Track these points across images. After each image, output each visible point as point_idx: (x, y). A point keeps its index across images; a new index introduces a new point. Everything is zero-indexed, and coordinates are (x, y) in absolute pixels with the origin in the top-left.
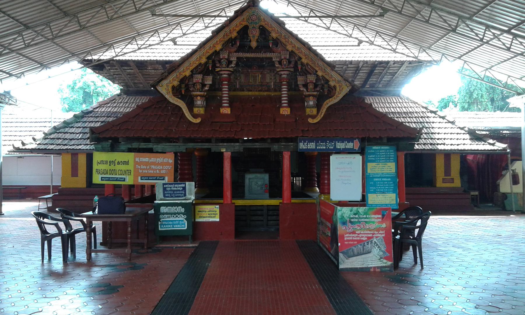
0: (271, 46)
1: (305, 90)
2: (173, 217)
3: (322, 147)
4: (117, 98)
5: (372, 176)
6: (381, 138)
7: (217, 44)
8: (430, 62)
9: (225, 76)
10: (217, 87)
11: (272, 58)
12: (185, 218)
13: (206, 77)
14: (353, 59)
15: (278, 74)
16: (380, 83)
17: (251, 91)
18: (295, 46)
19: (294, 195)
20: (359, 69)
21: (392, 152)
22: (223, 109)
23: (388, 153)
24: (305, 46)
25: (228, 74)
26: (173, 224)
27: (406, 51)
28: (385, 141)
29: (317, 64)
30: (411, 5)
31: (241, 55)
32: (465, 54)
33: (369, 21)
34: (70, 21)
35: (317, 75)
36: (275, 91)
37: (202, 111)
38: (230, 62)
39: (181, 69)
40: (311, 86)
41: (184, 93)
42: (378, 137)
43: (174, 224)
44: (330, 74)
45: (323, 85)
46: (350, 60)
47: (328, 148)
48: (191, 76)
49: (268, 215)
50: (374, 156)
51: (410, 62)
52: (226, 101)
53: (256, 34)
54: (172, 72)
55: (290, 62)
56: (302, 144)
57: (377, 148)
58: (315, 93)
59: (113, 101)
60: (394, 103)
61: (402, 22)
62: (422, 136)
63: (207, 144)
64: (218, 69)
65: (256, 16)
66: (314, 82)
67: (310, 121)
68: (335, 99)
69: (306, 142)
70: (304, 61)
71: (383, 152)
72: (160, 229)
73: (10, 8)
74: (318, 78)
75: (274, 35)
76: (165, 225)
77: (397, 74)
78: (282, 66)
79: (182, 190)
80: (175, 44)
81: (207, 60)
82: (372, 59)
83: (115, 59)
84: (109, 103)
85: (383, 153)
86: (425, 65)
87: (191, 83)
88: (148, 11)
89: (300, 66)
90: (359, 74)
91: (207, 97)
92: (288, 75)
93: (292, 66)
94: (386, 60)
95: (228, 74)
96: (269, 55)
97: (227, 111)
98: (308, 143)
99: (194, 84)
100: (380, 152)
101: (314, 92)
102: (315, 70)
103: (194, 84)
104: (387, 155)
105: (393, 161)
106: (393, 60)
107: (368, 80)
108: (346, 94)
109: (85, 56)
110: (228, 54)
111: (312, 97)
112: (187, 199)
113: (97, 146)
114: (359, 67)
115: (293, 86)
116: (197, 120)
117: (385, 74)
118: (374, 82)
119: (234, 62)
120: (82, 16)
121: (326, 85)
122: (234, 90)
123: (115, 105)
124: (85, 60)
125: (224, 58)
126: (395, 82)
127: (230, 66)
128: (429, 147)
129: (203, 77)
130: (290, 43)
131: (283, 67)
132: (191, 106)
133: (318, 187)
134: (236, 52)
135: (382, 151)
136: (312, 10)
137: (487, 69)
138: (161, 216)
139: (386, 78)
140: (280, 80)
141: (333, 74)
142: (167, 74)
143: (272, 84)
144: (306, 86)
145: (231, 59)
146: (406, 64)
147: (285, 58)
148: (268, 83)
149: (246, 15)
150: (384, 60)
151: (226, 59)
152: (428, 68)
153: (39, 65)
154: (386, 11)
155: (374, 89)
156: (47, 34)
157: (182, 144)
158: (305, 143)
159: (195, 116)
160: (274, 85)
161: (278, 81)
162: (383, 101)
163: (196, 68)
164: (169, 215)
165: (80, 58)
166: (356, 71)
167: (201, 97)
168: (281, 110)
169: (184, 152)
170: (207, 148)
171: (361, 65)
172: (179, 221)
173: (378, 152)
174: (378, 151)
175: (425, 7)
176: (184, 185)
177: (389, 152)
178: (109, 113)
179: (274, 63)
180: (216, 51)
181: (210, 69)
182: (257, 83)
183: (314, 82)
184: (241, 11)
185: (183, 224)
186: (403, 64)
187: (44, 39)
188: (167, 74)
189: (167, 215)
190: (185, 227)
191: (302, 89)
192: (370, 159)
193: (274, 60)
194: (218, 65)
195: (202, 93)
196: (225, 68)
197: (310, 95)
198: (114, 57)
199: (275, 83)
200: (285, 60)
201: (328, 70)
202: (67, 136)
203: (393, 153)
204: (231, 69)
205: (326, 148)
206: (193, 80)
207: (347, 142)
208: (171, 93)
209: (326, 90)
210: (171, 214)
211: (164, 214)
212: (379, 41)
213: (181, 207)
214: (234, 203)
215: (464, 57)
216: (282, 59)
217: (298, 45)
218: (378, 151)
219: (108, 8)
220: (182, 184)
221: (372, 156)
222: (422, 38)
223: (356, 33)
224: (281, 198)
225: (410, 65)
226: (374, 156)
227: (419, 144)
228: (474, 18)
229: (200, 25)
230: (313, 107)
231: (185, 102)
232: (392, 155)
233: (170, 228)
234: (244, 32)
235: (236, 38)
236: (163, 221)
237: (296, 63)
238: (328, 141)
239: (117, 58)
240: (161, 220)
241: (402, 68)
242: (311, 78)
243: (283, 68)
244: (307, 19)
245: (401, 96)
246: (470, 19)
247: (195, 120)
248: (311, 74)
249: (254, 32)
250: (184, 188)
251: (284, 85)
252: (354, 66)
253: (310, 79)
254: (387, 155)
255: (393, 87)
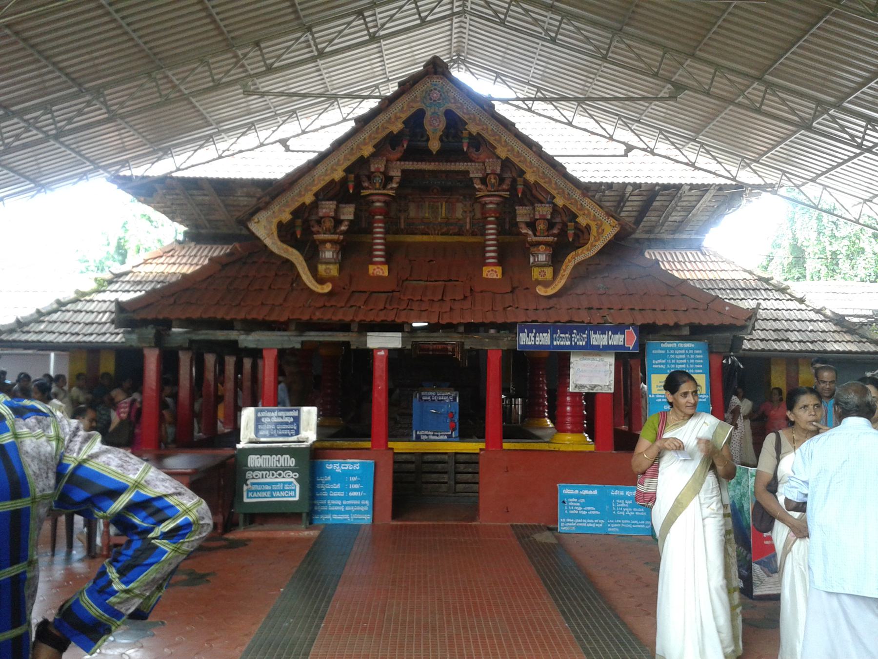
0: (465, 149)
1: (530, 233)
2: (273, 475)
3: (563, 341)
4: (178, 248)
5: (660, 400)
6: (677, 326)
7: (365, 144)
8: (758, 187)
9: (378, 204)
10: (364, 225)
11: (467, 172)
12: (295, 479)
13: (344, 206)
14: (615, 181)
15: (480, 202)
16: (663, 225)
17: (427, 234)
18: (513, 149)
19: (511, 433)
20: (625, 199)
21: (698, 354)
22: (375, 267)
23: (692, 356)
24: (531, 149)
25: (385, 202)
26: (272, 490)
27: (713, 166)
28: (686, 332)
29: (554, 182)
30: (729, 80)
31: (410, 165)
32: (823, 173)
33: (645, 111)
34: (89, 104)
35: (555, 205)
36: (473, 234)
37: (334, 270)
38: (388, 179)
39: (296, 190)
40: (541, 226)
41: (301, 235)
42: (672, 324)
43: (274, 491)
44: (579, 203)
45: (565, 225)
46: (609, 181)
47: (576, 343)
48: (315, 205)
49: (457, 473)
50: (664, 361)
51: (721, 188)
52: (378, 235)
53: (438, 125)
54: (277, 195)
55: (502, 180)
56: (525, 335)
57: (670, 345)
58: (550, 239)
59: (170, 254)
60: (690, 262)
61: (707, 112)
62: (757, 326)
63: (341, 334)
64: (365, 192)
65: (439, 91)
66: (549, 217)
67: (541, 291)
68: (588, 250)
69: (532, 332)
70: (531, 177)
71: (682, 354)
72: (246, 500)
73: (89, 151)
74: (555, 209)
75: (473, 129)
76: (257, 491)
77: (695, 209)
78: (487, 186)
79: (292, 423)
80: (287, 149)
81: (345, 174)
82: (649, 181)
83: (174, 175)
84: (161, 257)
85: (681, 356)
86: (747, 192)
87: (314, 217)
88: (239, 87)
89: (522, 187)
90: (625, 209)
91: (345, 243)
92: (497, 204)
93: (505, 187)
94: (677, 182)
95: (385, 202)
96: (461, 166)
97: (382, 271)
98: (535, 334)
99: (319, 222)
100: (675, 354)
101: (548, 236)
102: (551, 194)
103: (319, 222)
104: (689, 359)
105: (701, 371)
106: (688, 183)
107: (641, 221)
108: (609, 241)
109: (117, 171)
110: (385, 162)
111: (544, 247)
112: (301, 440)
113: (128, 336)
114: (624, 194)
115: (507, 226)
116: (325, 286)
117: (674, 209)
118: (654, 224)
119: (397, 180)
120: (111, 94)
121: (569, 224)
122: (397, 232)
123: (184, 261)
124: (119, 177)
125: (378, 170)
126: (692, 223)
127: (389, 187)
128: (758, 345)
129: (337, 206)
130: (503, 143)
131: (489, 188)
132: (312, 260)
133: (549, 418)
134: (400, 160)
135: (680, 352)
136: (539, 89)
137: (865, 201)
138: (249, 474)
139: (676, 217)
140: (482, 214)
141: (587, 202)
142: (268, 199)
143: (468, 220)
144: (532, 225)
145: (392, 174)
146: (712, 192)
147: (494, 173)
148: (459, 220)
149: (419, 91)
150: (672, 182)
151: (381, 172)
152: (753, 199)
153: (32, 185)
154: (679, 88)
155: (652, 236)
156: (47, 125)
157: (294, 333)
158: (530, 334)
159: (321, 281)
160: (470, 223)
161: (478, 215)
162: (670, 258)
163: (323, 189)
164: (264, 473)
165: (109, 172)
166: (619, 202)
167: (332, 245)
168: (486, 270)
169: (298, 349)
170: (343, 342)
171: (630, 189)
172: (284, 483)
173: (672, 354)
174: (672, 352)
175: (753, 83)
176: (297, 412)
177: (693, 354)
178: (160, 276)
179: (472, 181)
180: (362, 157)
181: (351, 191)
182: (439, 220)
183: (549, 217)
184: (411, 82)
185: (290, 490)
186: (707, 190)
187: (41, 136)
188: (268, 199)
189: (261, 473)
190: (295, 496)
191: (524, 231)
192: (656, 366)
193: (472, 175)
194: (366, 184)
195: (335, 237)
196: (380, 189)
197: (539, 244)
198: (172, 172)
199: (472, 218)
200: (492, 176)
201: (577, 194)
202: (80, 317)
203: (702, 356)
204: (391, 193)
205: (571, 343)
206: (317, 213)
207: (612, 333)
208: (275, 234)
209: (571, 232)
210: (269, 470)
211: (254, 470)
212: (663, 148)
213: (288, 456)
214: (392, 449)
215: (822, 178)
216: (488, 174)
217: (518, 146)
218: (672, 352)
219: (160, 79)
220: (292, 410)
221: (660, 361)
222: (745, 142)
223: (623, 135)
224: (483, 440)
225: (721, 193)
226: (664, 361)
227: (752, 339)
228: (846, 104)
229: (333, 115)
230: (544, 266)
231: (302, 254)
232: (698, 359)
233: (265, 497)
234: (416, 120)
235: (401, 132)
236: (253, 484)
237: (514, 181)
238: (575, 331)
239: (179, 174)
240: (249, 482)
241: (705, 197)
242: (544, 210)
243: (488, 191)
244: (529, 103)
245: (704, 250)
246: (838, 107)
247: (319, 286)
248: (541, 202)
249: (434, 122)
250: (297, 420)
251: (491, 223)
252: (616, 193)
253: (541, 213)
254: (689, 359)
255: (687, 232)
